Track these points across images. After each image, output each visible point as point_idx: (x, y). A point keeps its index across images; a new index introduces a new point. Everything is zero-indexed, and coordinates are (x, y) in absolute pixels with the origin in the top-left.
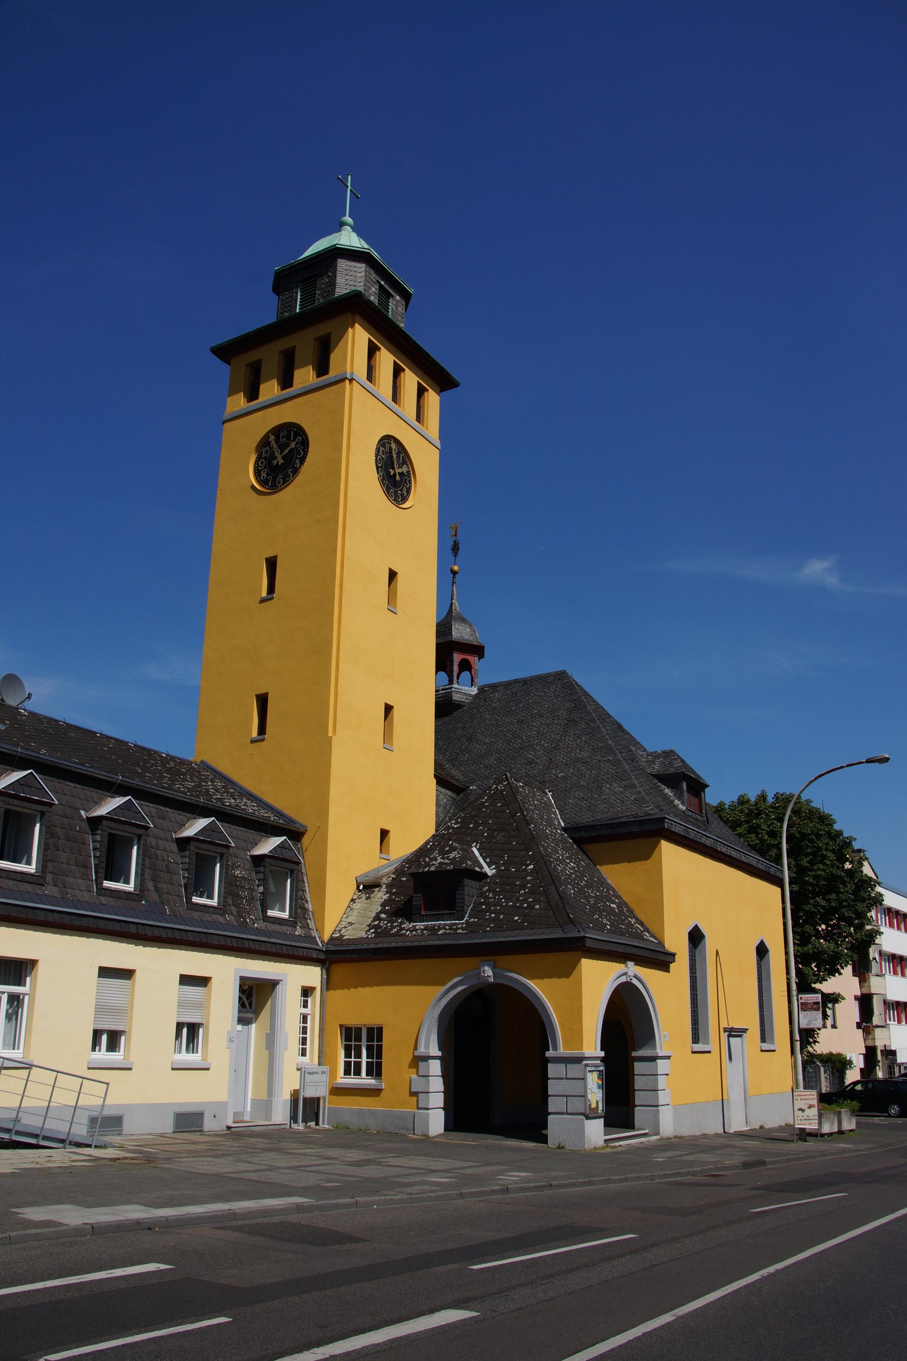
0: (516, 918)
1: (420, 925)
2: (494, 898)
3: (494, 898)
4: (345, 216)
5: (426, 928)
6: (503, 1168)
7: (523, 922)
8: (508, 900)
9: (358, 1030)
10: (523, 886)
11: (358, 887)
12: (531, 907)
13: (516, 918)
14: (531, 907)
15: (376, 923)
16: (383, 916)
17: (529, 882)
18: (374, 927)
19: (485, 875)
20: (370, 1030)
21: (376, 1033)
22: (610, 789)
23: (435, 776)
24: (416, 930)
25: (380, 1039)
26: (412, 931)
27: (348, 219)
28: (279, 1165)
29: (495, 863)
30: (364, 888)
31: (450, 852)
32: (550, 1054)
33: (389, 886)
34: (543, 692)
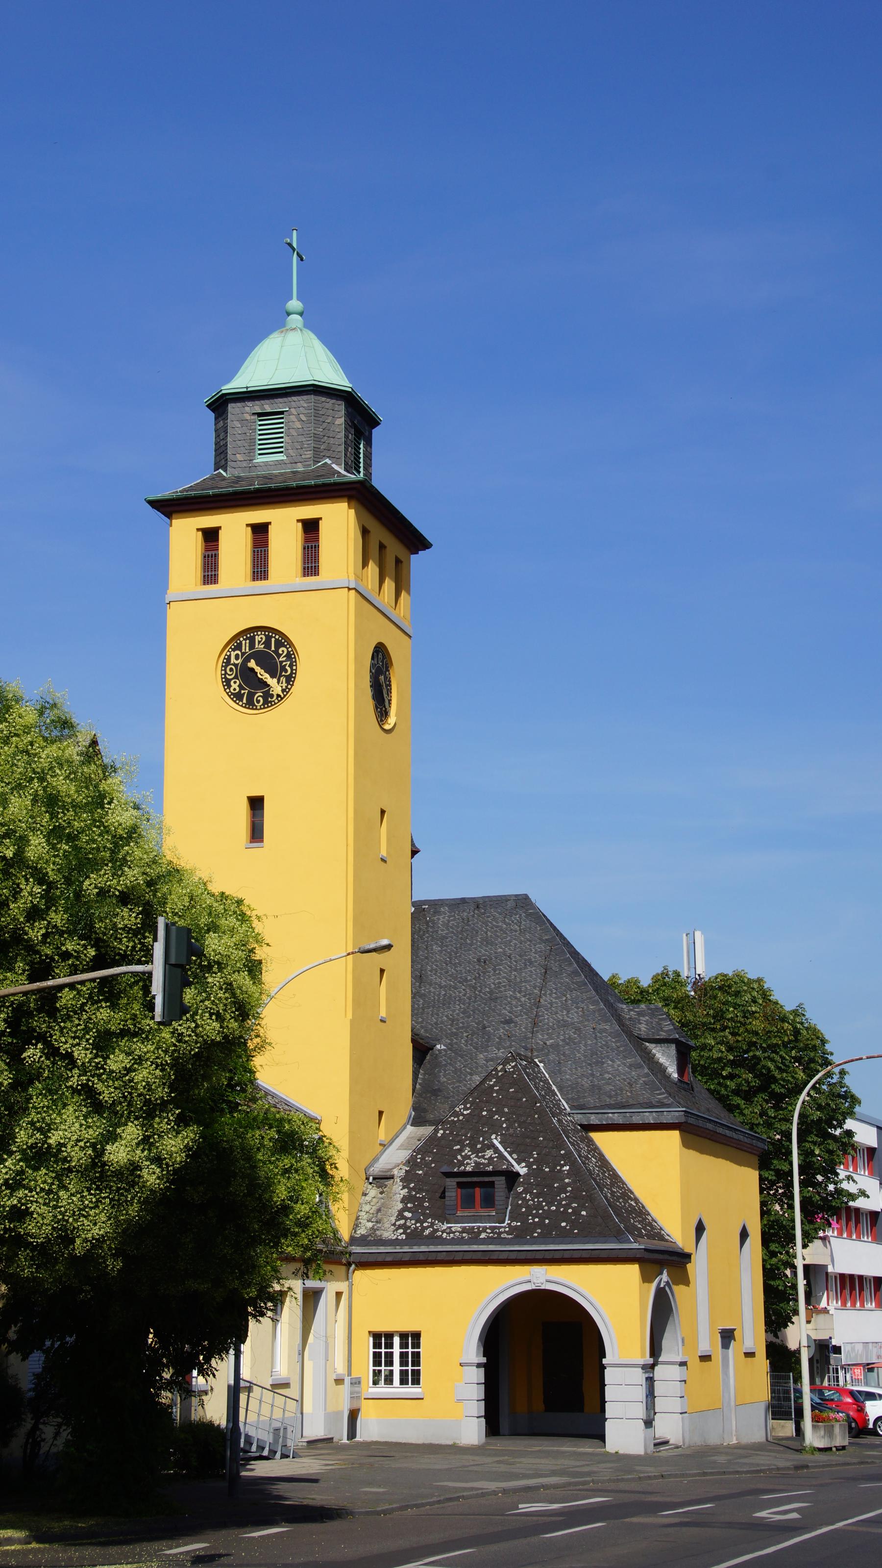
0: (563, 1224)
1: (456, 1227)
2: (533, 1200)
3: (533, 1200)
4: (291, 299)
5: (464, 1230)
6: (543, 1464)
7: (572, 1229)
8: (550, 1204)
9: (389, 1336)
10: (562, 1189)
11: (367, 1179)
12: (576, 1212)
13: (563, 1224)
14: (576, 1212)
15: (402, 1222)
16: (408, 1214)
17: (568, 1185)
18: (400, 1227)
19: (518, 1174)
20: (404, 1336)
21: (417, 1336)
22: (612, 1066)
23: (413, 1041)
24: (454, 1233)
25: (416, 1345)
26: (449, 1233)
27: (294, 304)
28: (739, 1469)
29: (524, 1161)
30: (374, 1179)
31: (483, 1150)
32: (604, 1361)
33: (406, 1180)
34: (505, 923)
